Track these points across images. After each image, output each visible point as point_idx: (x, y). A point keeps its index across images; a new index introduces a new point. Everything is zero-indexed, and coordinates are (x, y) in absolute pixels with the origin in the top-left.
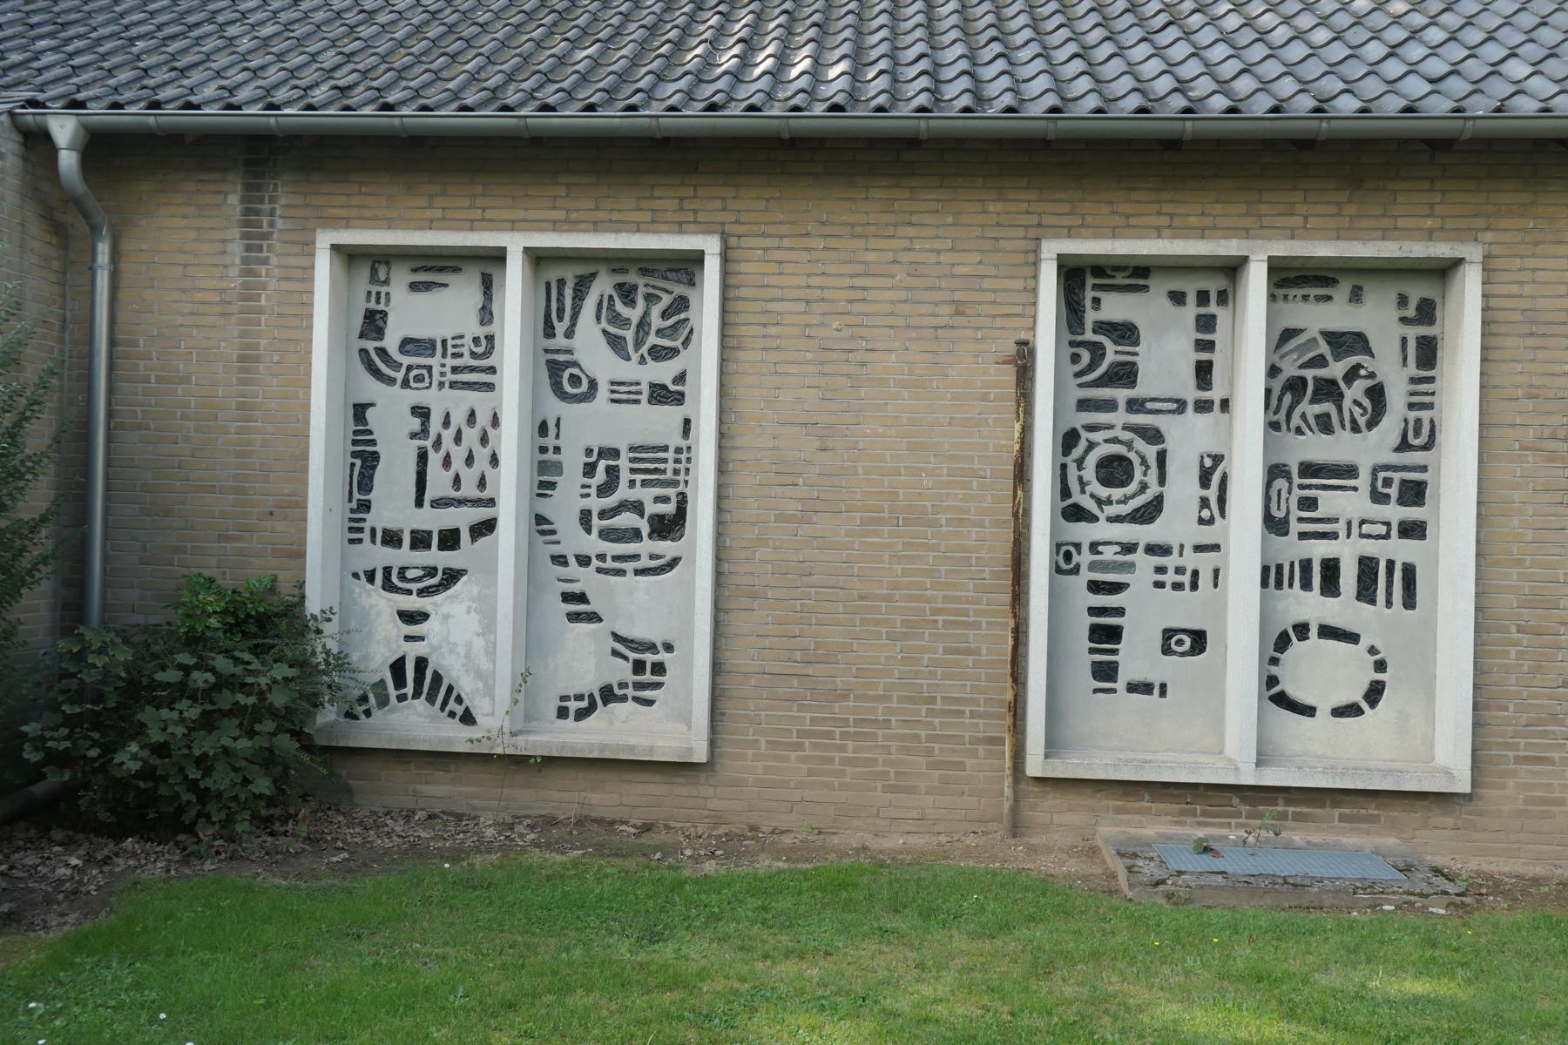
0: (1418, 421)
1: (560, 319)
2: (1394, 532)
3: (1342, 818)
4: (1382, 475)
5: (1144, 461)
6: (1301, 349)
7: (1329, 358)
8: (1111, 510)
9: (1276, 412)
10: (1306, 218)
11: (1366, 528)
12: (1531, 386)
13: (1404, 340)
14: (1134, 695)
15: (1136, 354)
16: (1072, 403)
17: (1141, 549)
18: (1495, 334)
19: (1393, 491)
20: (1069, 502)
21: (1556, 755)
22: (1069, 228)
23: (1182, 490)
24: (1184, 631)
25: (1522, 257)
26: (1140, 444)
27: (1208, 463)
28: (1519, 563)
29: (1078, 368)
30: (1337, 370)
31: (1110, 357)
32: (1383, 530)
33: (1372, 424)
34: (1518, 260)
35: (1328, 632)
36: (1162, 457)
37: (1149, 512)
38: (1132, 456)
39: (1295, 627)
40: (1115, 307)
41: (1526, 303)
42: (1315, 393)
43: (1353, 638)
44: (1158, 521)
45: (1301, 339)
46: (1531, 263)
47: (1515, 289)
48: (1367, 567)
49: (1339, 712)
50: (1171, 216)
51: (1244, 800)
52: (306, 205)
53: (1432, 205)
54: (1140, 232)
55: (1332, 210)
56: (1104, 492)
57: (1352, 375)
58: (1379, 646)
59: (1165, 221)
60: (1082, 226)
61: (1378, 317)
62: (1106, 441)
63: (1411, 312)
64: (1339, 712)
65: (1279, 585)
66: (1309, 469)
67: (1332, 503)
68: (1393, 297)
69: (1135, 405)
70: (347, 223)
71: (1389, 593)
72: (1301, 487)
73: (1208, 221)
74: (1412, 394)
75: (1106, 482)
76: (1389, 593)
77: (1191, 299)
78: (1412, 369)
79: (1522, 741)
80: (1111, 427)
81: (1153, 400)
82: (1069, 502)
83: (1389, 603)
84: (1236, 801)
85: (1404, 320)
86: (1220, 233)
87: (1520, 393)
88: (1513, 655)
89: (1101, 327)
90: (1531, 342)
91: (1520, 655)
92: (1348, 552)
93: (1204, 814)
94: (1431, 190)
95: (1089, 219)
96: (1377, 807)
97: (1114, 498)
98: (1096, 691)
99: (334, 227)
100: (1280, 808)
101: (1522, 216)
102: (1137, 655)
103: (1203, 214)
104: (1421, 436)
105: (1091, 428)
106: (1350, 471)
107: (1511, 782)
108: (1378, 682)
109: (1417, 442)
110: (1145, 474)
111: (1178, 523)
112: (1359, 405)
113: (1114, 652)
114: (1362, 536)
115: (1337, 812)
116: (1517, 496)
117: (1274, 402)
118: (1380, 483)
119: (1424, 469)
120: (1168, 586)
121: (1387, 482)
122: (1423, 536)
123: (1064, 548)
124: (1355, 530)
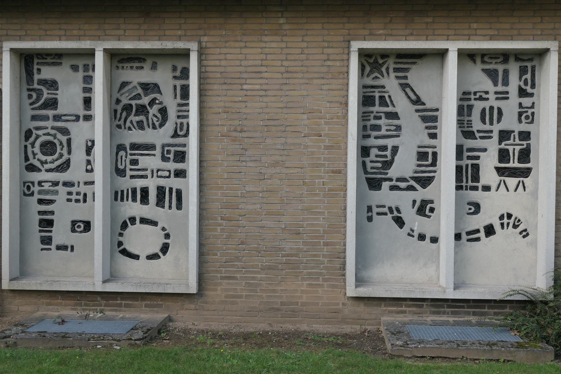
0: (182, 124)
2: (172, 175)
3: (146, 306)
4: (166, 148)
5: (61, 143)
6: (130, 91)
7: (142, 95)
8: (47, 166)
9: (119, 120)
10: (125, 31)
11: (160, 173)
12: (225, 107)
13: (175, 87)
14: (60, 251)
15: (57, 94)
16: (29, 117)
17: (61, 184)
18: (209, 84)
19: (171, 156)
20: (28, 163)
21: (238, 276)
22: (20, 36)
23: (78, 156)
24: (81, 221)
25: (220, 48)
26: (59, 136)
27: (90, 144)
28: (221, 188)
29: (31, 101)
30: (145, 101)
31: (45, 96)
32: (167, 174)
33: (161, 126)
34: (219, 49)
35: (144, 221)
36: (69, 141)
37: (65, 166)
38: (56, 141)
39: (130, 219)
40: (47, 73)
41: (222, 69)
42: (137, 111)
43: (155, 224)
44: (68, 171)
45: (130, 87)
46: (224, 51)
47: (217, 63)
48: (161, 191)
49: (150, 257)
50: (66, 30)
51: (103, 298)
52: (491, 28)
53: (180, 24)
54: (51, 37)
55: (137, 27)
56: (43, 158)
57: (152, 102)
58: (166, 227)
59: (62, 32)
60: (26, 35)
61: (162, 76)
62: (44, 134)
63: (178, 74)
64: (150, 257)
65: (122, 200)
66: (134, 146)
67: (145, 162)
68: (170, 67)
69: (57, 118)
70: (373, 36)
71: (170, 202)
72: (131, 155)
73: (82, 33)
74: (179, 111)
75: (44, 154)
76: (170, 202)
77: (81, 69)
78: (179, 100)
79: (224, 269)
80: (47, 128)
81: (65, 115)
82: (28, 163)
83: (170, 207)
84: (99, 299)
85: (175, 77)
86: (87, 38)
87: (220, 110)
88: (219, 231)
89: (40, 82)
90: (225, 87)
91: (222, 230)
92: (152, 184)
93: (86, 305)
94: (180, 17)
95: (29, 32)
96: (161, 301)
97: (48, 161)
98: (42, 249)
100: (118, 302)
101: (220, 29)
102: (60, 233)
103: (80, 29)
104: (182, 131)
105: (38, 128)
106: (152, 147)
107: (219, 288)
108: (166, 244)
109: (181, 133)
110: (62, 149)
111: (75, 173)
112: (156, 117)
113: (51, 231)
114: (158, 177)
115: (144, 303)
116: (220, 157)
117: (118, 116)
118: (165, 153)
119: (184, 146)
120: (73, 201)
121: (169, 152)
122: (185, 177)
123: (27, 184)
124: (155, 174)
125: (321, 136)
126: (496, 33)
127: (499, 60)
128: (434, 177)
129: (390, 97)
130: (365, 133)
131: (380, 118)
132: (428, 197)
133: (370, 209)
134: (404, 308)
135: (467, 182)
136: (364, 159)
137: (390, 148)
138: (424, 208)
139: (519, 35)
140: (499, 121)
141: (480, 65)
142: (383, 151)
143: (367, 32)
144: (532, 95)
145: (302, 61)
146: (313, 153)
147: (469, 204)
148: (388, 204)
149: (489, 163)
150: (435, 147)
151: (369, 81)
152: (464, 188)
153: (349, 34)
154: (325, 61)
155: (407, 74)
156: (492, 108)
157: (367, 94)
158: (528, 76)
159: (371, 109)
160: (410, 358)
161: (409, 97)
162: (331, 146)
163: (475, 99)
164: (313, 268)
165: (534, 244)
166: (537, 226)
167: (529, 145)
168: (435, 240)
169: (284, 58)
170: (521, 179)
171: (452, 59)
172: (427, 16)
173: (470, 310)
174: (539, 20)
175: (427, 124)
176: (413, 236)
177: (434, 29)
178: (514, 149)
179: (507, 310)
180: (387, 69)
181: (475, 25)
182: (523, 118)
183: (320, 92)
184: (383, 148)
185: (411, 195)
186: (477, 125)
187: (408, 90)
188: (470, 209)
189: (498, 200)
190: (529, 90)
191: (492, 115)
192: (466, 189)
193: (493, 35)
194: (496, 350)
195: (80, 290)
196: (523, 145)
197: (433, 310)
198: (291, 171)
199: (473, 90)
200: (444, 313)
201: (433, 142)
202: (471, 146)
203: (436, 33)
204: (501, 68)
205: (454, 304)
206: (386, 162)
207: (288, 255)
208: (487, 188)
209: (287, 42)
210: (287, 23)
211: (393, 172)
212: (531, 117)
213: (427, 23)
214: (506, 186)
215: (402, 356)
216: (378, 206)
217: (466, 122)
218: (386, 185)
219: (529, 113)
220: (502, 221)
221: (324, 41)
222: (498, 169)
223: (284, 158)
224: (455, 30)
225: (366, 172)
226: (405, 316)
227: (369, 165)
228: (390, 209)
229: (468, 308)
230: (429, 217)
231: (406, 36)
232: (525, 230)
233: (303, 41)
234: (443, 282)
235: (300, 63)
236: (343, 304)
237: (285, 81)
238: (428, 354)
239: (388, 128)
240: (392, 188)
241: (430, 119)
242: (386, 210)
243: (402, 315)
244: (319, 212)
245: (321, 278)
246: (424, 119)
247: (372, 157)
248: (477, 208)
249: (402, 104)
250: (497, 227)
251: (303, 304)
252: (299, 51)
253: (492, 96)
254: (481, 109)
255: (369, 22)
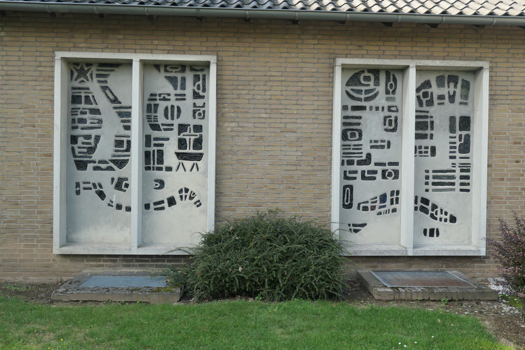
1: (353, 90)
52: (168, 45)
70: (76, 48)
99: (418, 59)
125: (35, 127)
126: (172, 48)
127: (178, 70)
128: (128, 160)
129: (93, 96)
130: (74, 125)
131: (86, 113)
132: (123, 176)
133: (78, 185)
134: (102, 263)
135: (154, 164)
136: (73, 145)
137: (93, 137)
138: (121, 184)
139: (190, 50)
140: (178, 117)
141: (163, 74)
142: (88, 139)
143: (71, 45)
144: (203, 97)
145: (19, 66)
146: (28, 140)
147: (156, 181)
148: (92, 181)
149: (170, 149)
150: (129, 137)
151: (77, 84)
152: (152, 169)
153: (286, 67)
154: (37, 67)
155: (106, 79)
156: (172, 107)
157: (75, 94)
158: (200, 82)
159: (78, 106)
160: (67, 302)
161: (108, 97)
162: (43, 135)
163: (160, 100)
164: (28, 232)
165: (205, 212)
166: (207, 198)
167: (201, 136)
168: (128, 209)
169: (5, 64)
170: (195, 162)
171: (136, 67)
172: (119, 34)
173: (153, 263)
174: (205, 39)
175: (122, 119)
176: (112, 206)
177: (124, 44)
178: (190, 139)
179: (183, 263)
180: (91, 75)
181: (156, 41)
182: (197, 114)
183: (34, 91)
184: (88, 137)
185: (109, 174)
186: (161, 120)
187: (108, 92)
188: (156, 185)
189: (178, 177)
190: (201, 93)
191: (173, 112)
192: (153, 170)
193: (170, 50)
194: (135, 294)
195: (440, 255)
196: (197, 136)
197: (125, 263)
198: (11, 155)
199: (158, 92)
200: (133, 266)
201: (127, 132)
202: (157, 136)
203: (126, 47)
204: (179, 76)
205: (141, 259)
206: (91, 148)
207: (8, 222)
208: (169, 169)
209: (6, 51)
210: (7, 36)
211: (96, 156)
212: (203, 114)
213: (119, 39)
214: (184, 167)
215: (61, 301)
216: (84, 183)
217: (153, 118)
218: (90, 166)
219: (201, 111)
220: (181, 194)
221: (37, 51)
222: (178, 154)
223: (5, 144)
224: (141, 45)
225: (75, 156)
226: (103, 269)
227: (77, 150)
228: (94, 185)
229: (152, 262)
230: (125, 191)
231: (102, 49)
232: (199, 201)
233: (20, 51)
234: (403, 243)
235: (17, 68)
236: (53, 260)
237: (5, 82)
238: (81, 299)
239: (92, 121)
240: (96, 168)
241: (124, 114)
242: (90, 185)
243: (100, 268)
244: (34, 187)
245: (35, 239)
246: (120, 114)
247: (79, 144)
248: (161, 184)
249: (103, 103)
250: (177, 199)
251: (21, 261)
252: (17, 58)
253: (173, 98)
254: (165, 107)
255: (73, 37)
